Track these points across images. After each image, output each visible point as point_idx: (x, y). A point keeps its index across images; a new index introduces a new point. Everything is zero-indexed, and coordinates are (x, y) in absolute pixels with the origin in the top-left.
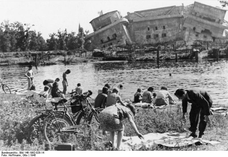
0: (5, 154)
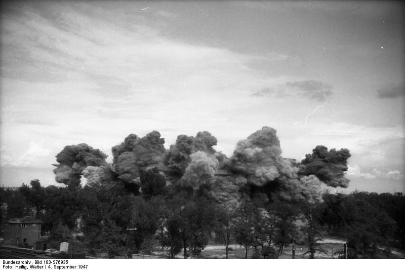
0: (10, 265)
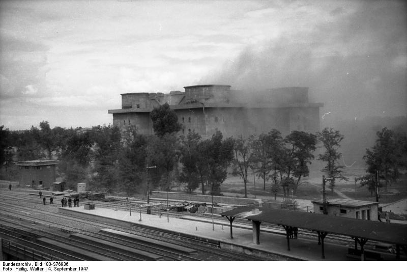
0: (10, 267)
